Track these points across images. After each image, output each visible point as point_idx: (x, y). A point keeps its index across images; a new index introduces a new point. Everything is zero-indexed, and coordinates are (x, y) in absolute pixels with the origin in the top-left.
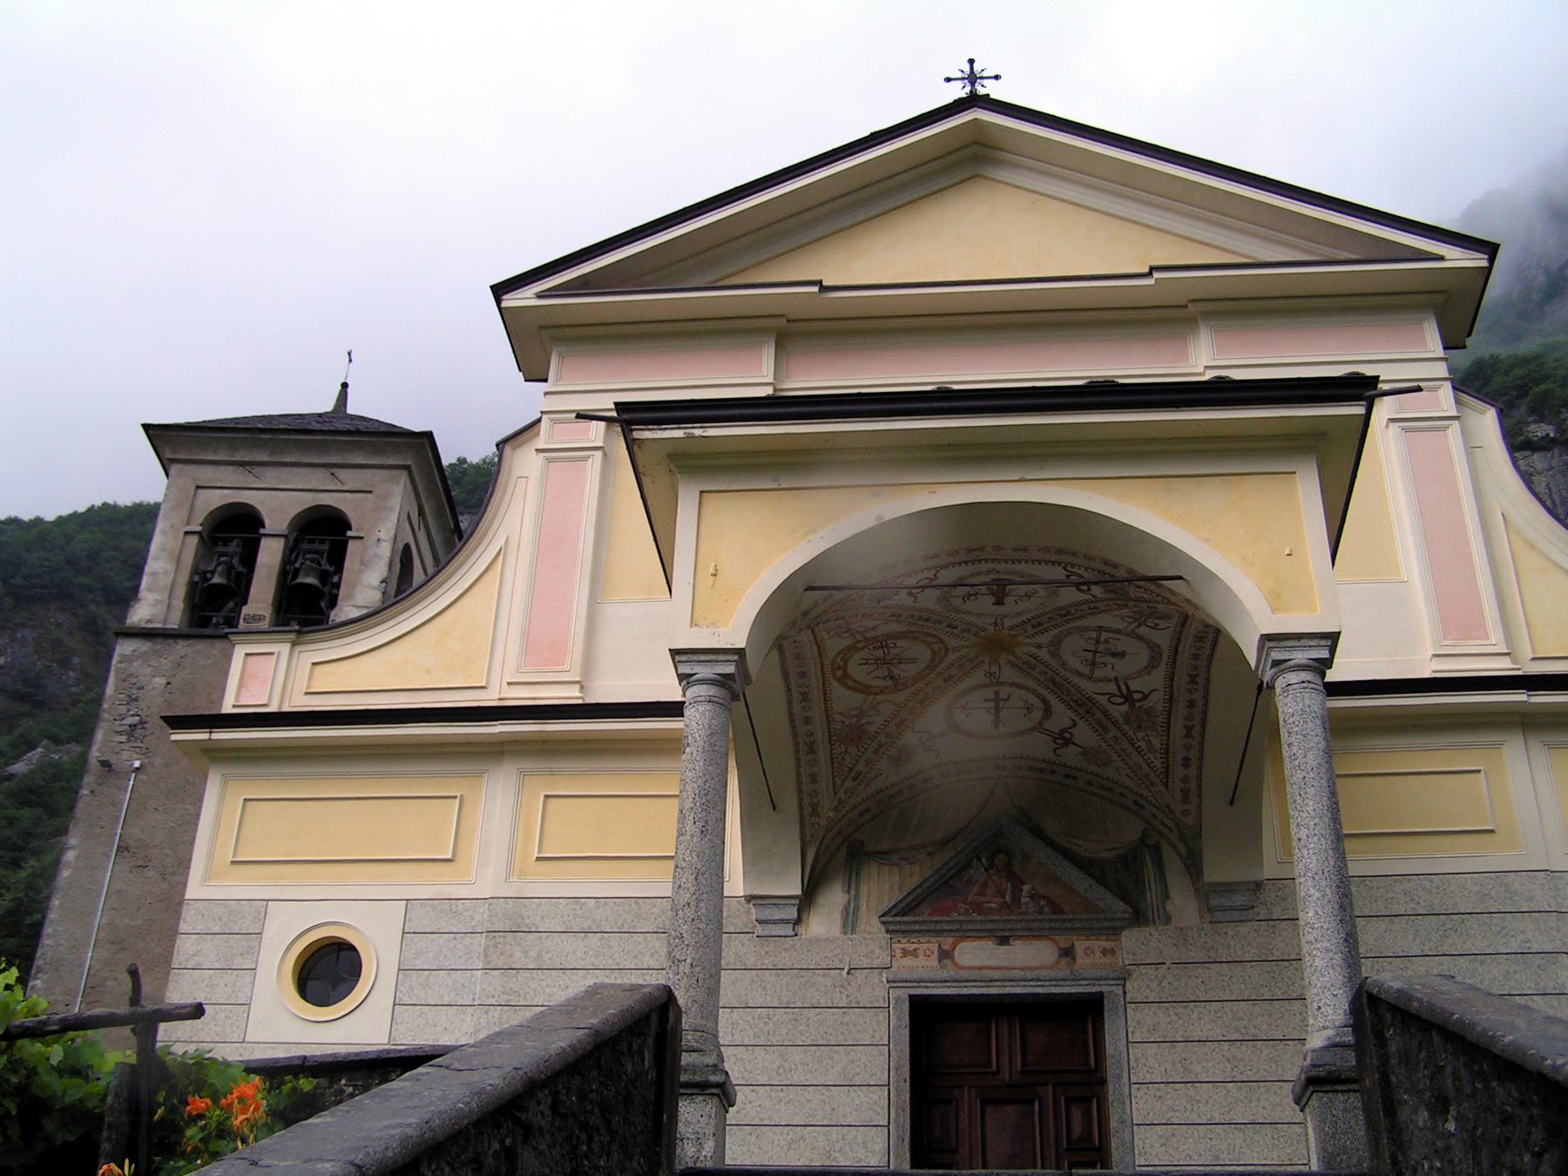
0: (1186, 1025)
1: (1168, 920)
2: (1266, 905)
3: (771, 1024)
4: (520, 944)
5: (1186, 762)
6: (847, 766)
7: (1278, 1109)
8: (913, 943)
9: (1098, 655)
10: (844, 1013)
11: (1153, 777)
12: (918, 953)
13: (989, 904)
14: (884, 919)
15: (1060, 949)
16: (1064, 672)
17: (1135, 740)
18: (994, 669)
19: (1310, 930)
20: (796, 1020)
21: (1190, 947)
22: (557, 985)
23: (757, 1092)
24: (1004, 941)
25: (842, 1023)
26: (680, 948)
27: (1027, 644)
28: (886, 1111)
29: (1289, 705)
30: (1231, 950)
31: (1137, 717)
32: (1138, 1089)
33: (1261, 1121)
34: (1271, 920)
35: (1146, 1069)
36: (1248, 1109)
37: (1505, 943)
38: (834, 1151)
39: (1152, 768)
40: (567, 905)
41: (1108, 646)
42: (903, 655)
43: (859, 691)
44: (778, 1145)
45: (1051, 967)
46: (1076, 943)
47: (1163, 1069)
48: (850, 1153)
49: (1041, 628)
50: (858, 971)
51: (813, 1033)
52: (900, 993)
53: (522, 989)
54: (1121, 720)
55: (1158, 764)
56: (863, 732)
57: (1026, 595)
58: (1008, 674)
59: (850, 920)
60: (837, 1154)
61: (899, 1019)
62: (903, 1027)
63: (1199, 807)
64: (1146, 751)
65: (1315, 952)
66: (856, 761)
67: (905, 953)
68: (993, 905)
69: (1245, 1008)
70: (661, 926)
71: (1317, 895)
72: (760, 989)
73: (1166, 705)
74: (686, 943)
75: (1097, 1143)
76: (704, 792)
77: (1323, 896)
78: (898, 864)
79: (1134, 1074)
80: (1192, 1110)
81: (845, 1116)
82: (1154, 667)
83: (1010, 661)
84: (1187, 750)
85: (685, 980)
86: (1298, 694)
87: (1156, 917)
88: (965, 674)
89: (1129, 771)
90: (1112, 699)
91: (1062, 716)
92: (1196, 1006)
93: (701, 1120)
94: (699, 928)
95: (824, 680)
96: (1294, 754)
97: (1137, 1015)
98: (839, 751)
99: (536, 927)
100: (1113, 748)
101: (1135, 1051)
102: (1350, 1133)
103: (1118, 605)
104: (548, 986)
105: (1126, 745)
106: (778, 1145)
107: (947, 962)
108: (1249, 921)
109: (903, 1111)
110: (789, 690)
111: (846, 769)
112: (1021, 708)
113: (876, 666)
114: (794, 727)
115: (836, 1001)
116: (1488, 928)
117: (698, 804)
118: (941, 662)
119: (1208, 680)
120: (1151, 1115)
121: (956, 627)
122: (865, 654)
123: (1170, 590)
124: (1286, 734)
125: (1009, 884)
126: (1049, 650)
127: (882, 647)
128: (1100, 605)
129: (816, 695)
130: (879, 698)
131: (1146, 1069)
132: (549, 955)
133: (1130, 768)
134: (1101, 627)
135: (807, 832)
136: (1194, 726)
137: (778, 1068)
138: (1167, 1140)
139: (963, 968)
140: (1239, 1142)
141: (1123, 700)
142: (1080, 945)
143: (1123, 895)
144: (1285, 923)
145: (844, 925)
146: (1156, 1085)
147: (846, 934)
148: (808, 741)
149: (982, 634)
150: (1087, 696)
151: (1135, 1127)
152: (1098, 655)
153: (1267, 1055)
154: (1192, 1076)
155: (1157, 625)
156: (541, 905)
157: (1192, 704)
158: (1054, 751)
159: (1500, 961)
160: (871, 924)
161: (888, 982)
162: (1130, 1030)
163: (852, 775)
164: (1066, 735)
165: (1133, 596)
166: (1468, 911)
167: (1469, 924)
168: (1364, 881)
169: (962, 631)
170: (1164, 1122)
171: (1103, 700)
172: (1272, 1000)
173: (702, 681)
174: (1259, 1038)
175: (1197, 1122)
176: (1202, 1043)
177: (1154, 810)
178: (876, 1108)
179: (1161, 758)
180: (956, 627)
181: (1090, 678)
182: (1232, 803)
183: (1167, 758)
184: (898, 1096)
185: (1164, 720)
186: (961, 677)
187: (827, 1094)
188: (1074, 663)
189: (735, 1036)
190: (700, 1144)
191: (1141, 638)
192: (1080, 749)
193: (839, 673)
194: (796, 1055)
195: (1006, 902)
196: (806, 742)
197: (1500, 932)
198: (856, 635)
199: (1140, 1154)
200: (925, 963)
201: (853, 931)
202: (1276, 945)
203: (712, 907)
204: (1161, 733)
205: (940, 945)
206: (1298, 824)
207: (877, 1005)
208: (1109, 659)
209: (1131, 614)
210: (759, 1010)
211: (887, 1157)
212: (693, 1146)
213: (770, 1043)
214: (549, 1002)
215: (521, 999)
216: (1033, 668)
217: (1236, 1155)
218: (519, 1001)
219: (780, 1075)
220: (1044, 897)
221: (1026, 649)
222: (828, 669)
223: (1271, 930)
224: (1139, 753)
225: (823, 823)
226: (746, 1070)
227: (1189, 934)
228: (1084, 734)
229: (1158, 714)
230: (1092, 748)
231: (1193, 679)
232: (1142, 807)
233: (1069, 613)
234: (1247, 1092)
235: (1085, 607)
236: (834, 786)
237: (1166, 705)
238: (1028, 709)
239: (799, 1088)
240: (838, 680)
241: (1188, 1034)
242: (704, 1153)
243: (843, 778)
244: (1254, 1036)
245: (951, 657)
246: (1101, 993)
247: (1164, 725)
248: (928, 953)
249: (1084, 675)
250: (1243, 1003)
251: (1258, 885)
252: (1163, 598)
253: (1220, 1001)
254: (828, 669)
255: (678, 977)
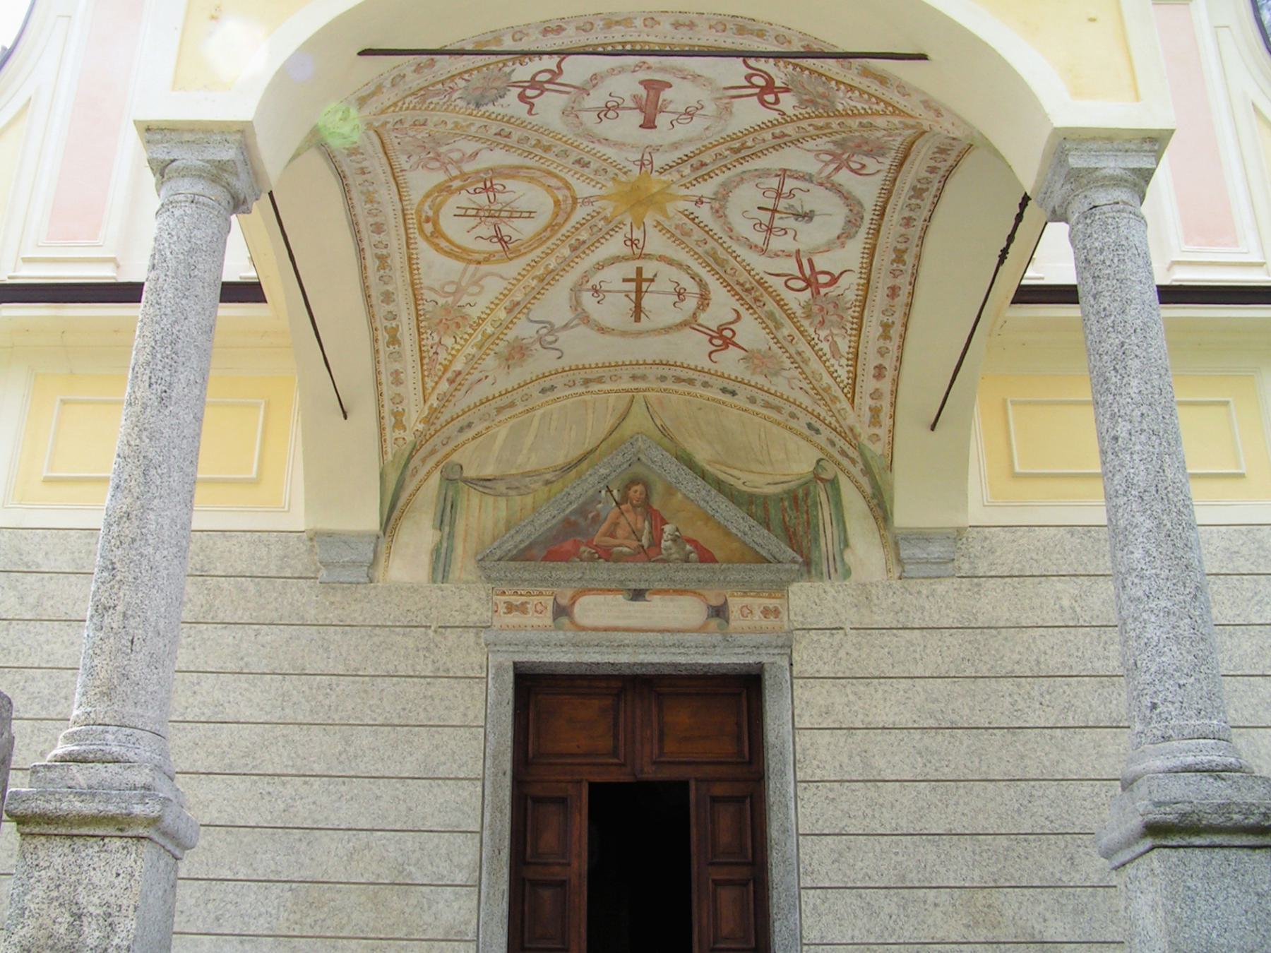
0: (867, 706)
1: (847, 573)
2: (970, 557)
3: (334, 697)
4: (15, 588)
5: (879, 372)
6: (440, 364)
7: (980, 816)
8: (521, 595)
9: (777, 215)
10: (428, 684)
11: (836, 391)
12: (507, 608)
13: (620, 548)
14: (483, 564)
15: (709, 607)
16: (729, 242)
17: (816, 340)
18: (638, 234)
19: (1136, 581)
20: (366, 692)
21: (874, 609)
22: (60, 640)
23: (312, 785)
24: (638, 595)
25: (425, 697)
26: (108, 585)
27: (685, 198)
28: (479, 812)
29: (1096, 236)
30: (925, 613)
31: (821, 309)
32: (805, 788)
33: (959, 832)
34: (976, 577)
35: (815, 763)
36: (944, 816)
37: (1258, 611)
38: (409, 865)
39: (835, 379)
40: (79, 538)
41: (791, 202)
42: (514, 205)
43: (457, 257)
44: (336, 855)
45: (700, 630)
46: (729, 600)
47: (837, 764)
48: (429, 867)
49: (704, 171)
50: (449, 630)
51: (387, 709)
52: (501, 659)
53: (13, 645)
54: (799, 312)
55: (843, 373)
56: (463, 317)
57: (686, 113)
58: (656, 243)
59: (441, 564)
60: (413, 869)
61: (499, 693)
62: (504, 703)
63: (892, 431)
64: (829, 355)
65: (1145, 616)
66: (454, 356)
67: (510, 608)
68: (625, 549)
69: (942, 687)
70: (198, 567)
71: (1149, 524)
72: (321, 651)
73: (860, 293)
74: (118, 578)
75: (750, 855)
76: (169, 338)
77: (1158, 527)
78: (507, 495)
79: (801, 769)
80: (874, 816)
81: (424, 818)
82: (849, 236)
83: (658, 223)
84: (882, 355)
85: (112, 640)
86: (1110, 221)
87: (832, 571)
88: (598, 241)
89: (804, 384)
90: (790, 283)
91: (722, 306)
92: (880, 684)
93: (116, 882)
94: (142, 555)
95: (408, 238)
96: (1105, 309)
97: (806, 693)
98: (430, 342)
99: (38, 565)
100: (787, 351)
101: (803, 739)
102: (1217, 917)
103: (817, 128)
104: (48, 642)
105: (803, 346)
106: (336, 855)
107: (564, 620)
108: (948, 577)
109: (501, 812)
110: (361, 251)
111: (440, 367)
112: (670, 293)
113: (478, 220)
114: (369, 306)
115: (418, 668)
116: (1237, 593)
117: (159, 356)
118: (566, 220)
119: (919, 257)
120: (820, 822)
121: (587, 165)
122: (463, 199)
123: (903, 90)
124: (1090, 280)
125: (646, 523)
126: (712, 208)
127: (486, 189)
128: (789, 129)
129: (398, 260)
130: (484, 268)
131: (815, 763)
132: (52, 602)
133: (806, 378)
134: (785, 170)
135: (389, 450)
136: (893, 323)
137: (340, 754)
138: (840, 855)
139: (583, 629)
140: (931, 857)
141: (803, 284)
142: (735, 604)
143: (791, 537)
144: (992, 581)
145: (434, 570)
146: (828, 784)
147: (434, 582)
148: (389, 326)
149: (623, 178)
150: (757, 277)
151: (801, 838)
152: (777, 215)
153: (968, 747)
154: (875, 773)
155: (863, 166)
156: (46, 537)
157: (894, 292)
158: (710, 356)
159: (1252, 634)
160: (463, 566)
161: (487, 645)
162: (796, 712)
163: (449, 374)
164: (727, 333)
165: (840, 107)
166: (1214, 572)
167: (1215, 587)
168: (1089, 531)
169: (596, 172)
170: (837, 831)
171: (778, 283)
172: (975, 677)
173: (184, 173)
174: (959, 725)
175: (879, 832)
176: (887, 731)
177: (833, 436)
178: (466, 808)
179: (847, 365)
180: (587, 165)
181: (763, 252)
182: (933, 427)
183: (855, 366)
184: (495, 793)
185: (856, 314)
186: (593, 245)
187: (403, 789)
188: (744, 228)
189: (287, 710)
190: (110, 925)
191: (837, 189)
192: (743, 353)
193: (428, 228)
194: (364, 738)
195: (643, 547)
196: (386, 327)
197: (1252, 597)
198: (450, 167)
199: (806, 873)
200: (536, 622)
201: (445, 579)
202: (980, 608)
203: (168, 521)
204: (849, 332)
205: (555, 599)
206: (1113, 415)
207: (473, 675)
208: (791, 223)
209: (830, 147)
210: (318, 678)
211: (477, 874)
212: (99, 928)
213: (330, 722)
214: (48, 662)
215: (12, 659)
216: (687, 234)
217: (927, 875)
218: (8, 661)
219: (341, 763)
220: (690, 541)
221: (682, 205)
222: (412, 222)
223: (976, 590)
224: (820, 358)
225: (410, 438)
226: (298, 756)
227: (873, 592)
228: (750, 332)
229: (848, 305)
230: (759, 351)
231: (899, 256)
232: (817, 431)
233: (743, 146)
234: (942, 794)
235: (767, 135)
236: (424, 389)
237: (860, 293)
238: (679, 294)
239: (367, 780)
240: (427, 239)
241: (869, 719)
242: (116, 941)
243: (436, 379)
244: (952, 723)
245: (580, 213)
246: (761, 666)
247: (855, 320)
248: (539, 608)
249: (756, 246)
250: (940, 680)
251: (957, 535)
252: (887, 104)
253: (912, 678)
254: (412, 222)
255: (101, 635)
